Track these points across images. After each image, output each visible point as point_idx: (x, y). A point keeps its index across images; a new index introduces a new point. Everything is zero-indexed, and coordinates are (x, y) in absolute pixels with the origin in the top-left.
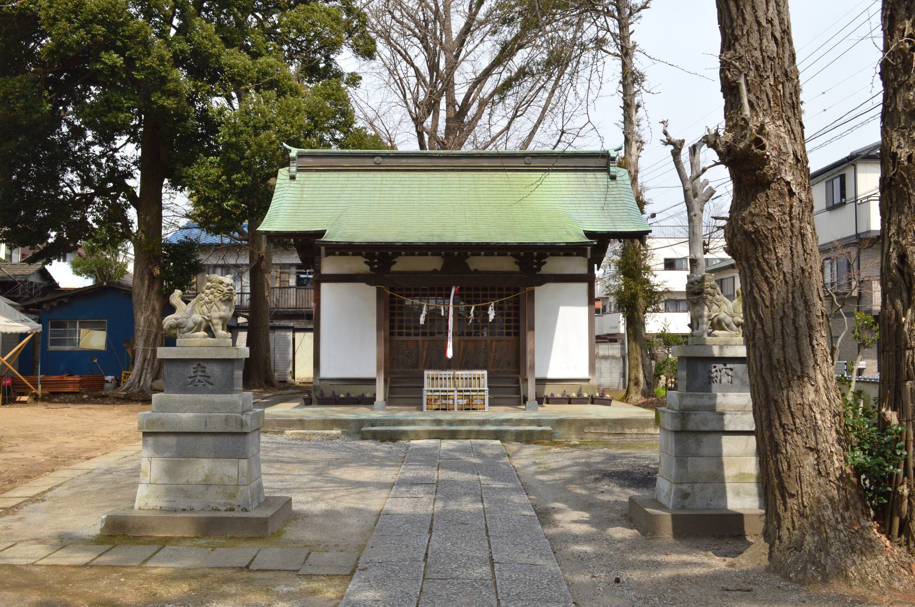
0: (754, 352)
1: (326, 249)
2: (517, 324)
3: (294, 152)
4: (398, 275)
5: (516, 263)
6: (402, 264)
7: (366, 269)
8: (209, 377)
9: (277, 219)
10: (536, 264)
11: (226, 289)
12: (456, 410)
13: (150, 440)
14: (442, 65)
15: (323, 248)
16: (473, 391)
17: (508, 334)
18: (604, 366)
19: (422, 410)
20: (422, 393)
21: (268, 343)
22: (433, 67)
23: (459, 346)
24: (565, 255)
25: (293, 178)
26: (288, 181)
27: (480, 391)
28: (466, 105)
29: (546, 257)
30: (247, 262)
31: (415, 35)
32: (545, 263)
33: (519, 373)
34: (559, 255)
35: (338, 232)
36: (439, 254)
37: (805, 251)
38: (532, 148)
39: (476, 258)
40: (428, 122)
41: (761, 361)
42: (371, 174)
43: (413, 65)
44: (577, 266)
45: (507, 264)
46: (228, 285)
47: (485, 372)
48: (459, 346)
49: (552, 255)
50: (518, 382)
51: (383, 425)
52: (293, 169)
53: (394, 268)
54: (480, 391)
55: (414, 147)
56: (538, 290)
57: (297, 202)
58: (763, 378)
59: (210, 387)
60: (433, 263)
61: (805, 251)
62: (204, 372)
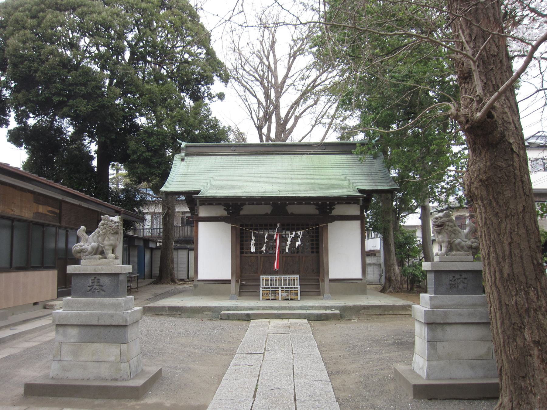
0: (489, 268)
1: (200, 201)
2: (316, 247)
3: (184, 144)
4: (244, 216)
5: (316, 208)
6: (246, 210)
7: (225, 213)
8: (102, 286)
9: (172, 184)
10: (328, 209)
11: (114, 226)
12: (280, 300)
13: (61, 330)
14: (273, 96)
15: (198, 200)
16: (291, 288)
17: (312, 252)
18: (369, 270)
19: (259, 300)
20: (259, 289)
21: (172, 258)
22: (267, 96)
23: (282, 260)
24: (347, 203)
25: (183, 160)
26: (180, 162)
27: (295, 288)
28: (286, 121)
29: (334, 205)
30: (161, 211)
31: (258, 80)
32: (334, 208)
33: (319, 276)
34: (343, 204)
35: (208, 192)
36: (270, 204)
37: (525, 193)
38: (326, 141)
39: (292, 205)
40: (265, 130)
41: (495, 275)
42: (229, 157)
43: (256, 97)
44: (354, 210)
45: (311, 210)
46: (115, 223)
47: (298, 276)
48: (282, 260)
49: (338, 203)
50: (318, 281)
51: (234, 310)
52: (183, 155)
53: (242, 213)
54: (295, 288)
55: (257, 141)
56: (330, 225)
57: (187, 173)
58: (497, 287)
59: (103, 293)
60: (266, 209)
61: (525, 193)
62: (98, 282)
